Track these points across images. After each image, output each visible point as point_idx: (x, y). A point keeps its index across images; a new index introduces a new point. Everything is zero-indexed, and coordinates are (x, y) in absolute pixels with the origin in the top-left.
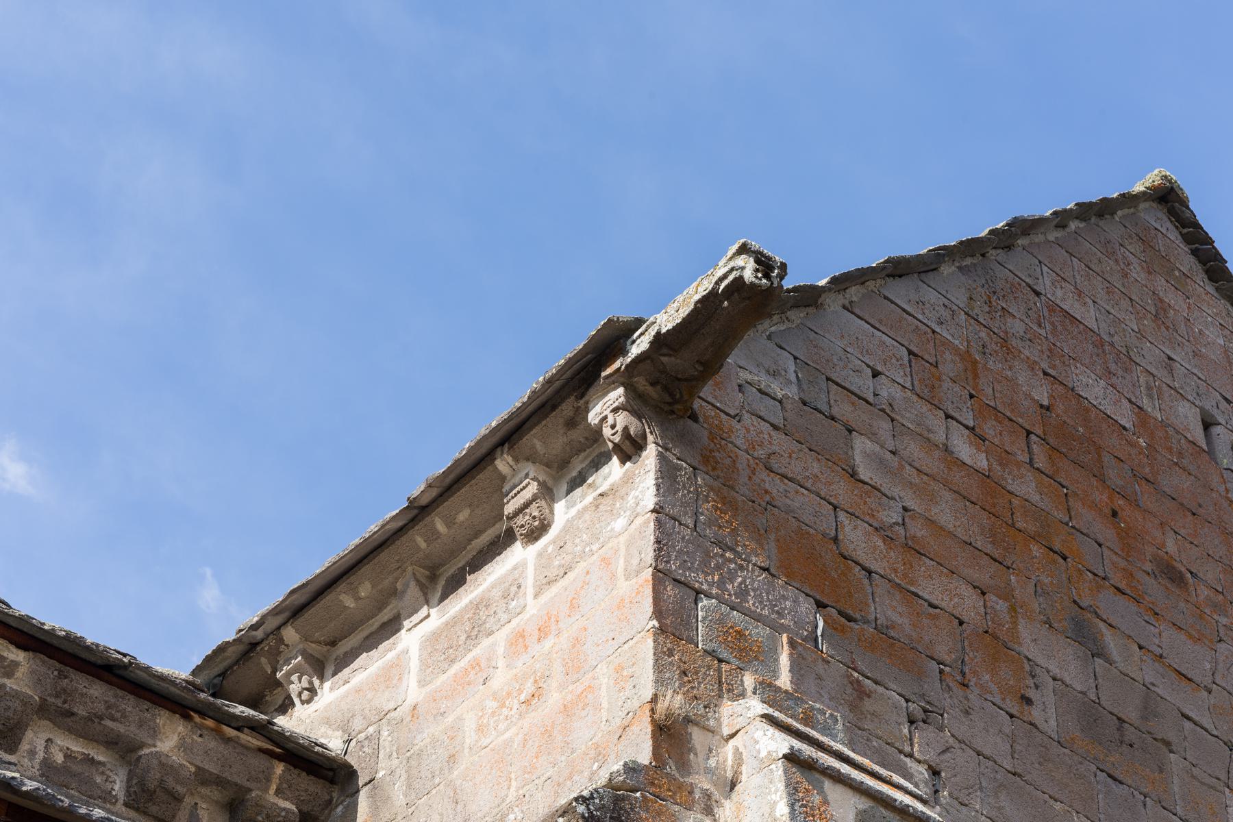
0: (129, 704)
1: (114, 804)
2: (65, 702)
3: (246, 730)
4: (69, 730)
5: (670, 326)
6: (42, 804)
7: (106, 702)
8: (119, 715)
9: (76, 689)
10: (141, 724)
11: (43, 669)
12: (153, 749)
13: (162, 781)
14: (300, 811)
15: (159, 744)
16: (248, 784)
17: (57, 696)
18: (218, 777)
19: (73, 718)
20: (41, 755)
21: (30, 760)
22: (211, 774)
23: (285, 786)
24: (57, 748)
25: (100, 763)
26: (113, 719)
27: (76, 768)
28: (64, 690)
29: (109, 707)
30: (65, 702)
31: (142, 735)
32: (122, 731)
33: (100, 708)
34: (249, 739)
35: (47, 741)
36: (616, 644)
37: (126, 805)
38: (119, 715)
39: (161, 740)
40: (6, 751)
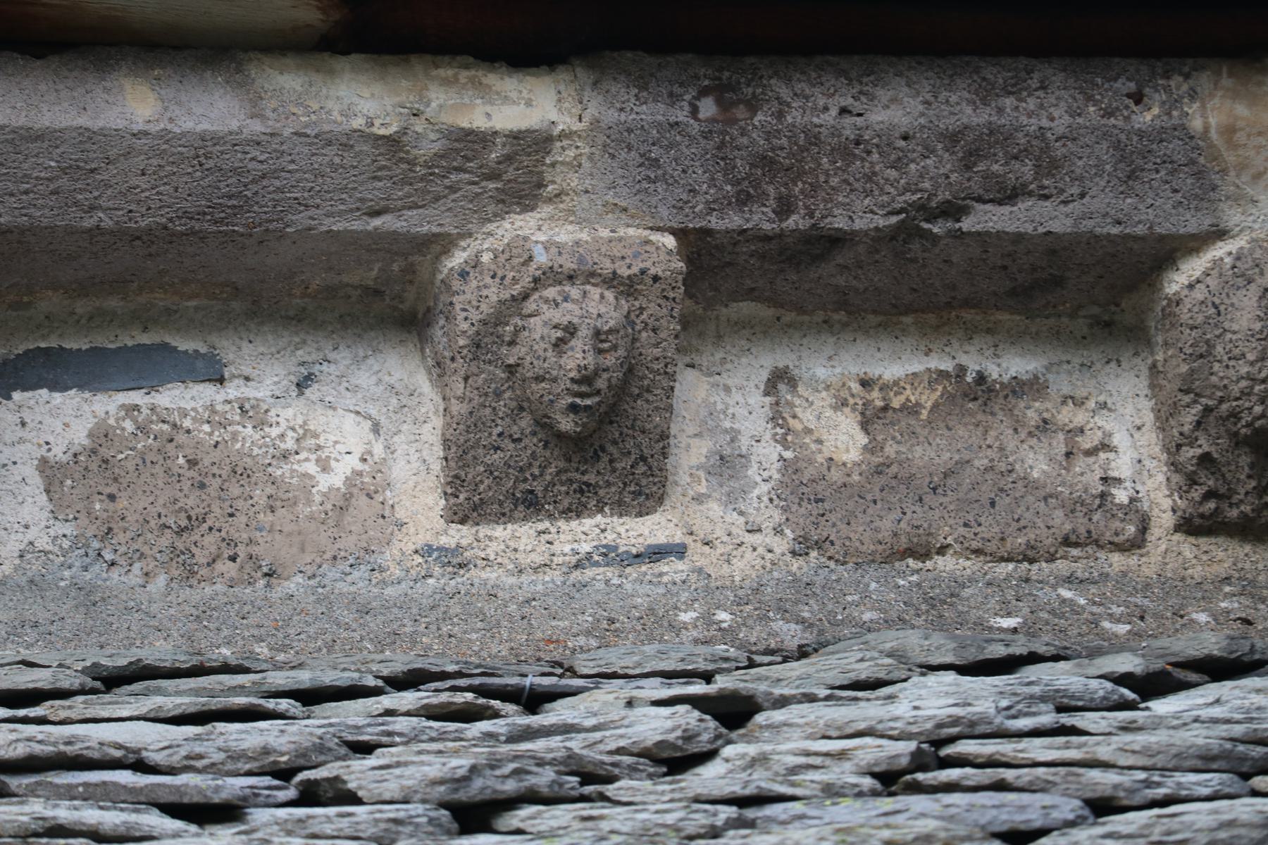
1: (1136, 544)
2: (785, 208)
4: (843, 304)
5: (40, 391)
7: (952, 138)
9: (814, 138)
10: (1133, 162)
11: (652, 112)
17: (743, 200)
19: (843, 257)
20: (767, 455)
21: (732, 500)
24: (823, 400)
26: (1009, 195)
27: (927, 454)
28: (766, 163)
30: (785, 208)
32: (1062, 225)
33: (937, 173)
35: (771, 388)
37: (1189, 526)
38: (1026, 170)
39: (1238, 199)
40: (621, 509)
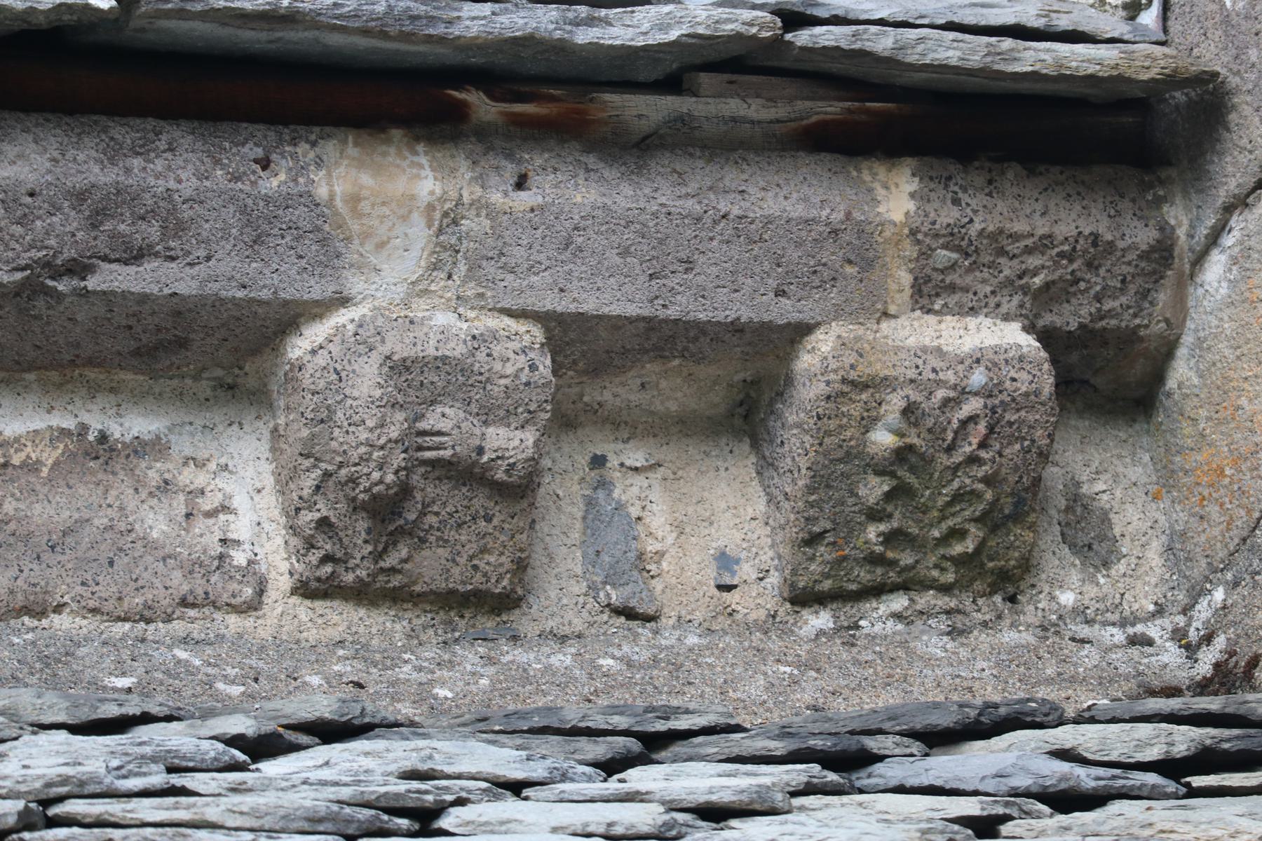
0: (178, 169)
1: (252, 607)
3: (705, 78)
6: (384, 35)
7: (79, 197)
8: (153, 231)
12: (342, 317)
13: (415, 438)
14: (1047, 337)
15: (355, 284)
16: (785, 311)
18: (651, 324)
22: (618, 323)
23: (944, 256)
25: (141, 448)
26: (136, 256)
29: (95, 221)
31: (279, 277)
34: (734, 106)
36: (458, 721)
37: (306, 590)
